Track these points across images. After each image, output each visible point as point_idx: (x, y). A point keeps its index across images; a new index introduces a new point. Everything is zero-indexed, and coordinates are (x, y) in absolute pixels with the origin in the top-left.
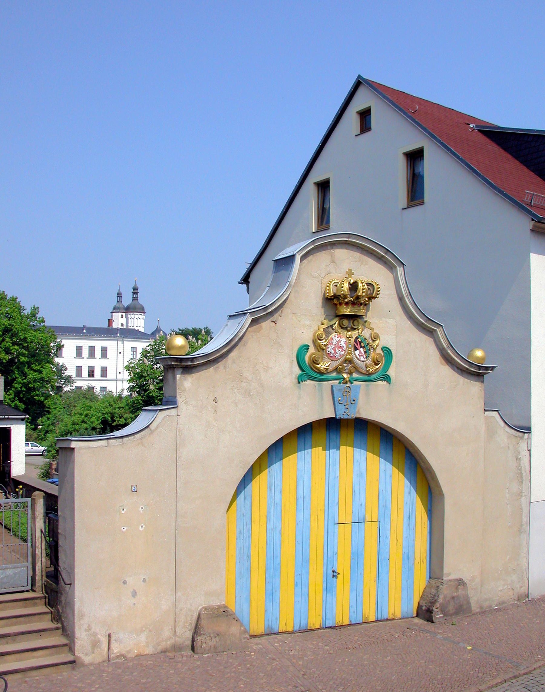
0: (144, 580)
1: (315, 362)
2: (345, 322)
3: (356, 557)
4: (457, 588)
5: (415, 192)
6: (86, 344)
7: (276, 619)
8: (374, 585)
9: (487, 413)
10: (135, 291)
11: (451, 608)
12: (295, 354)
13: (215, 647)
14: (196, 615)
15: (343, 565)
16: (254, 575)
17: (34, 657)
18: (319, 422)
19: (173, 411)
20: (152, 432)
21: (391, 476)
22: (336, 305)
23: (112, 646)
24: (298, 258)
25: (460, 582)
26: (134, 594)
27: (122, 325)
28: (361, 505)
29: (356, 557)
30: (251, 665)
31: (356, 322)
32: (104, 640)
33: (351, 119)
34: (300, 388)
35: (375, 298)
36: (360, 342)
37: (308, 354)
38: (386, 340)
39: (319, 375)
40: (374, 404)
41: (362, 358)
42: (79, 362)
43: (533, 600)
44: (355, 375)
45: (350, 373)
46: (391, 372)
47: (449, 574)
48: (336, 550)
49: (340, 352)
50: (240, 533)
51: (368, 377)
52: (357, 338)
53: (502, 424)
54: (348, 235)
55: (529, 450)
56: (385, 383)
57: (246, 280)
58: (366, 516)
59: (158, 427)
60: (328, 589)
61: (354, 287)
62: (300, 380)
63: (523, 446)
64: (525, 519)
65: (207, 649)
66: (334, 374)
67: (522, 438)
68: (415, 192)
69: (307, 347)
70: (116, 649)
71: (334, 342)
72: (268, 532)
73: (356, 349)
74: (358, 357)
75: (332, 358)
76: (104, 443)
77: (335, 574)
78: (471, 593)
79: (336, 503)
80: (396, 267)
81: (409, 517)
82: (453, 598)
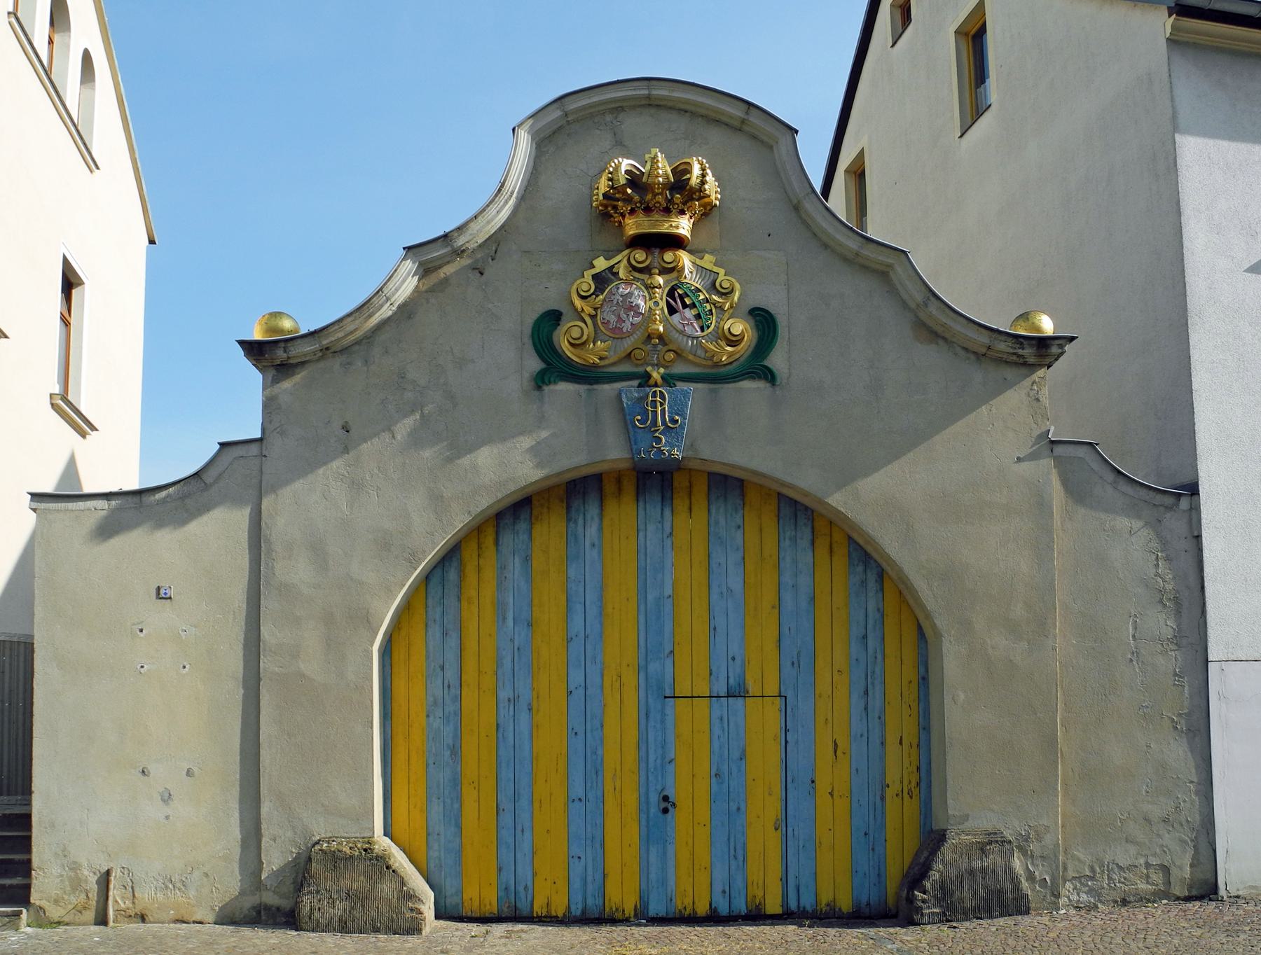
0: (189, 773)
7: (526, 888)
8: (774, 840)
9: (1059, 450)
15: (691, 786)
16: (469, 795)
20: (207, 487)
26: (167, 798)
28: (733, 659)
39: (588, 376)
50: (435, 703)
51: (716, 376)
53: (1110, 476)
54: (646, 83)
59: (219, 477)
62: (541, 380)
65: (323, 922)
67: (1169, 508)
69: (554, 317)
72: (501, 705)
74: (680, 327)
79: (667, 652)
81: (866, 692)
82: (973, 872)
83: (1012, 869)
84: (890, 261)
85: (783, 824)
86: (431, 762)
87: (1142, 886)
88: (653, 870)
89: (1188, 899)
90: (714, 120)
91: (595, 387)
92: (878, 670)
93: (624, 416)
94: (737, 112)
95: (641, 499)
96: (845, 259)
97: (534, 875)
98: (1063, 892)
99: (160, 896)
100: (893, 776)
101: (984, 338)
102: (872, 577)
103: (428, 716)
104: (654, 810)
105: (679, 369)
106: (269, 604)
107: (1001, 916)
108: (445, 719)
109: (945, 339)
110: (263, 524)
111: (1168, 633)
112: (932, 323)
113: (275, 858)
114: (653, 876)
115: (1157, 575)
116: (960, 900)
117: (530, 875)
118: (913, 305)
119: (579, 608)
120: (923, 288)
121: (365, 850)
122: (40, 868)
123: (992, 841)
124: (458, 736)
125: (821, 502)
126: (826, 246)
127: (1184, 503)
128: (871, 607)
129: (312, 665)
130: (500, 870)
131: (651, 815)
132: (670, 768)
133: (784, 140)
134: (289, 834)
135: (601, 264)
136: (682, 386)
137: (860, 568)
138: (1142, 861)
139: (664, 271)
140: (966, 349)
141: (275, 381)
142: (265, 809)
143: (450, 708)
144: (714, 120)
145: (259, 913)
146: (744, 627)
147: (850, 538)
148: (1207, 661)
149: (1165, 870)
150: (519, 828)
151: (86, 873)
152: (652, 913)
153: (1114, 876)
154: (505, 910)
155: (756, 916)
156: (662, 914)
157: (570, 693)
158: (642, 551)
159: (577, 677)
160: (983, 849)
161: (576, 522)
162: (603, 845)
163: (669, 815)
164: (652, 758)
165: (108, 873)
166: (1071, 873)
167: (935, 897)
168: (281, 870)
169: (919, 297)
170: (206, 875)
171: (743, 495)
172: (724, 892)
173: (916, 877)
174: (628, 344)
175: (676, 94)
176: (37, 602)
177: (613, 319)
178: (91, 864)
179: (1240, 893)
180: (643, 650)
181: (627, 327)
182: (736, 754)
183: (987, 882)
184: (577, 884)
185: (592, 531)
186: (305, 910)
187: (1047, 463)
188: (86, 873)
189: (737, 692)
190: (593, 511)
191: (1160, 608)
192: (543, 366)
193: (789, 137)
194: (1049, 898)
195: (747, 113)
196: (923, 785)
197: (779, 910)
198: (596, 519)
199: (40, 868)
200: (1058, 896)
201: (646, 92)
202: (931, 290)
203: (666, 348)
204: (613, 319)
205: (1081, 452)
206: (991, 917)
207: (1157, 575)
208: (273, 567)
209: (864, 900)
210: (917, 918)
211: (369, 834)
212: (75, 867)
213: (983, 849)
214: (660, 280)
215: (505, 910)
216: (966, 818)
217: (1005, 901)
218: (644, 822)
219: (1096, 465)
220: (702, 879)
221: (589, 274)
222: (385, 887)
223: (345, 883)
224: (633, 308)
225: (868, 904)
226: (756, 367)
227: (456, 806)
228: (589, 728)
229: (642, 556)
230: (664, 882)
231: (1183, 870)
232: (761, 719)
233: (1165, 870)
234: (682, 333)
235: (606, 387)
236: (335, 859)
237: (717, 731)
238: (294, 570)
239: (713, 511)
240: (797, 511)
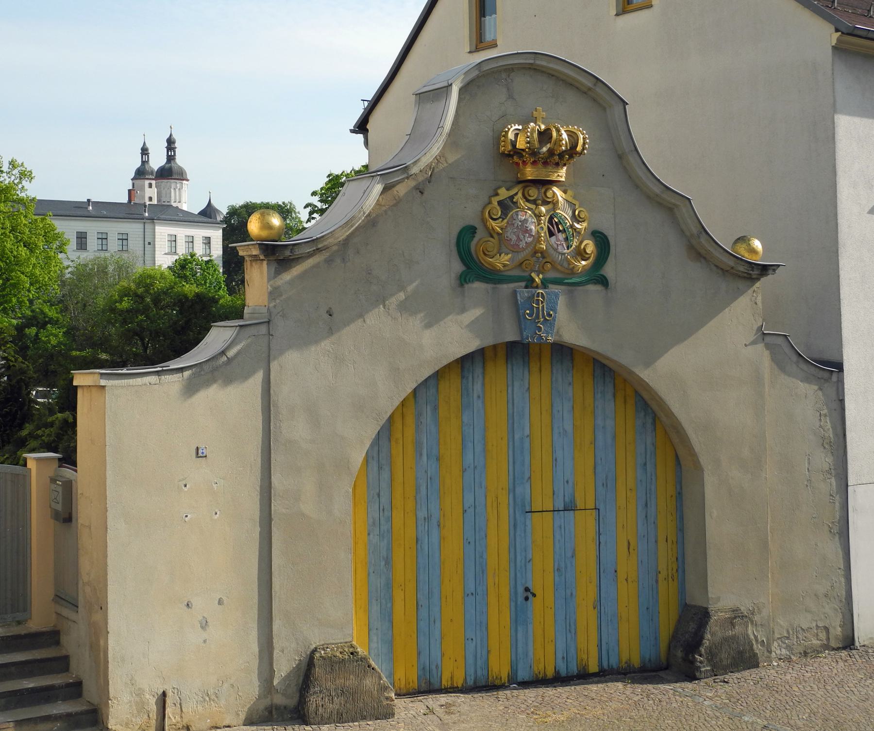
0: (220, 602)
2: (533, 192)
4: (733, 625)
7: (437, 666)
8: (593, 615)
9: (768, 339)
10: (171, 144)
11: (724, 657)
12: (454, 241)
15: (541, 579)
16: (398, 596)
22: (518, 164)
26: (204, 625)
28: (567, 482)
39: (492, 277)
46: (609, 270)
48: (529, 556)
50: (374, 523)
51: (567, 280)
53: (795, 358)
56: (598, 288)
57: (362, 127)
58: (577, 495)
60: (519, 618)
62: (463, 280)
65: (326, 715)
67: (826, 380)
69: (468, 232)
74: (555, 246)
76: (153, 379)
81: (646, 505)
82: (726, 639)
83: (748, 635)
84: (678, 203)
85: (598, 604)
86: (371, 571)
87: (815, 642)
88: (520, 645)
89: (838, 649)
90: (569, 84)
91: (498, 286)
92: (653, 488)
93: (518, 310)
94: (588, 83)
95: (509, 362)
96: (649, 197)
97: (443, 655)
98: (773, 649)
99: (200, 708)
100: (662, 566)
101: (731, 262)
102: (649, 420)
103: (369, 534)
104: (520, 599)
105: (552, 275)
106: (277, 459)
107: (744, 669)
108: (381, 536)
109: (705, 258)
110: (272, 392)
111: (826, 467)
112: (698, 247)
113: (285, 665)
114: (520, 650)
115: (821, 426)
116: (721, 660)
117: (439, 654)
118: (688, 234)
119: (470, 445)
120: (698, 225)
121: (352, 653)
122: (115, 698)
123: (736, 616)
124: (390, 549)
125: (632, 373)
126: (637, 186)
127: (834, 378)
128: (649, 441)
129: (308, 507)
130: (419, 653)
131: (519, 603)
132: (529, 566)
134: (294, 645)
135: (504, 194)
137: (642, 414)
138: (814, 625)
139: (545, 203)
140: (716, 266)
141: (278, 273)
142: (277, 625)
143: (384, 527)
144: (569, 84)
145: (271, 712)
146: (574, 459)
147: (636, 392)
148: (847, 486)
149: (827, 629)
150: (432, 620)
151: (148, 696)
152: (520, 679)
153: (800, 636)
154: (423, 685)
155: (583, 677)
156: (526, 679)
157: (465, 511)
158: (511, 401)
159: (469, 499)
160: (731, 622)
161: (467, 378)
162: (487, 628)
163: (529, 602)
164: (519, 558)
165: (164, 694)
166: (777, 635)
167: (707, 658)
168: (288, 676)
169: (694, 230)
170: (232, 686)
171: (572, 360)
172: (563, 658)
173: (693, 645)
174: (521, 256)
175: (551, 65)
176: (108, 467)
177: (514, 238)
178: (151, 687)
179: (865, 643)
180: (511, 477)
181: (522, 244)
182: (569, 554)
183: (734, 646)
184: (471, 661)
185: (478, 387)
186: (312, 707)
187: (760, 347)
188: (148, 696)
189: (570, 507)
190: (478, 371)
191: (822, 449)
192: (463, 268)
193: (621, 107)
194: (766, 654)
195: (595, 85)
196: (680, 571)
198: (481, 376)
199: (115, 698)
200: (770, 652)
201: (532, 61)
202: (703, 227)
203: (545, 260)
204: (514, 238)
206: (738, 671)
207: (821, 426)
208: (280, 427)
209: (647, 657)
210: (697, 674)
211: (350, 639)
212: (140, 693)
213: (731, 622)
214: (543, 209)
215: (423, 685)
216: (718, 599)
217: (745, 659)
218: (513, 609)
219: (787, 350)
220: (550, 649)
221: (495, 201)
222: (369, 682)
223: (340, 682)
224: (527, 231)
225: (650, 660)
226: (597, 277)
227: (389, 605)
228: (477, 538)
229: (510, 405)
231: (837, 631)
232: (584, 524)
233: (827, 629)
234: (556, 250)
235: (505, 286)
236: (333, 663)
237: (558, 537)
238: (294, 429)
239: (554, 371)
240: (604, 372)
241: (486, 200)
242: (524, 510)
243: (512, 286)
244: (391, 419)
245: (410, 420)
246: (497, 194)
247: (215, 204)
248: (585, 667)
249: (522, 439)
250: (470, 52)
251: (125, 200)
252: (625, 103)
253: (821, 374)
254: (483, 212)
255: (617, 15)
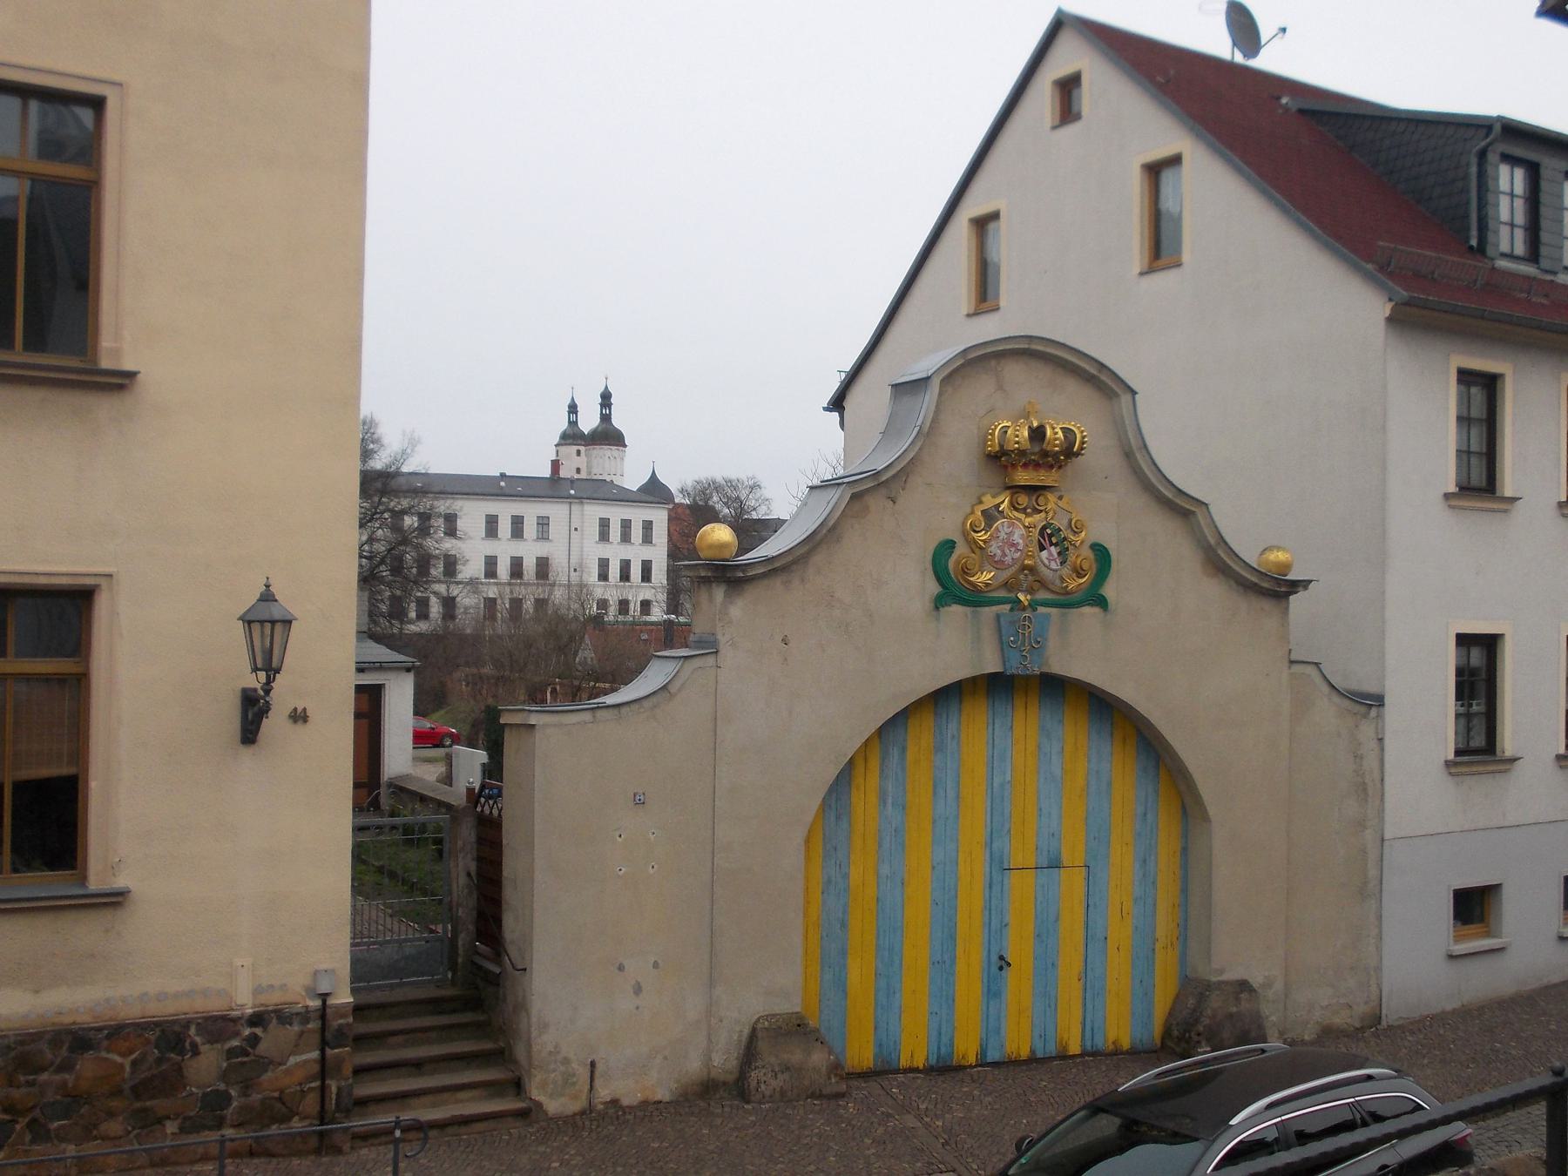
0: (656, 965)
1: (965, 571)
2: (1023, 500)
3: (1045, 933)
4: (1238, 999)
5: (1161, 247)
6: (505, 511)
9: (1297, 668)
10: (606, 398)
12: (930, 557)
13: (783, 1093)
14: (746, 1031)
15: (1020, 948)
17: (457, 1101)
18: (974, 680)
19: (710, 660)
20: (672, 696)
21: (1110, 784)
23: (597, 1082)
24: (936, 382)
25: (1243, 986)
26: (638, 990)
27: (578, 471)
29: (1045, 933)
30: (849, 1124)
31: (1041, 500)
32: (584, 1073)
33: (1043, 94)
34: (938, 619)
35: (1078, 454)
36: (1050, 536)
37: (954, 557)
38: (1100, 529)
39: (975, 598)
40: (1080, 650)
41: (1054, 566)
42: (490, 548)
43: (1390, 1027)
44: (1043, 595)
45: (1030, 591)
46: (1109, 591)
47: (1222, 971)
49: (1011, 555)
51: (1067, 602)
52: (1044, 528)
53: (1325, 689)
55: (1381, 740)
56: (1096, 610)
60: (993, 992)
61: (1038, 434)
62: (939, 603)
63: (1367, 731)
64: (1373, 873)
65: (768, 1093)
66: (1002, 594)
67: (1365, 716)
68: (1161, 247)
69: (949, 546)
70: (604, 1093)
71: (1002, 535)
73: (1042, 548)
75: (998, 565)
76: (587, 716)
77: (1004, 963)
78: (1266, 1010)
80: (1117, 395)
82: (1231, 1016)
85: (1084, 976)
100: (1161, 932)
104: (994, 969)
105: (1043, 595)
127: (1373, 712)
133: (1125, 398)
135: (989, 502)
136: (1041, 610)
189: (1055, 864)
197: (1078, 1052)
205: (1310, 670)
230: (998, 1031)
232: (1072, 883)
241: (968, 510)
242: (1001, 866)
243: (994, 608)
244: (851, 762)
245: (874, 763)
246: (981, 502)
247: (662, 478)
248: (1065, 1048)
249: (1002, 785)
250: (968, 315)
251: (546, 472)
252: (1134, 393)
253: (1358, 708)
254: (964, 523)
255: (1142, 274)
